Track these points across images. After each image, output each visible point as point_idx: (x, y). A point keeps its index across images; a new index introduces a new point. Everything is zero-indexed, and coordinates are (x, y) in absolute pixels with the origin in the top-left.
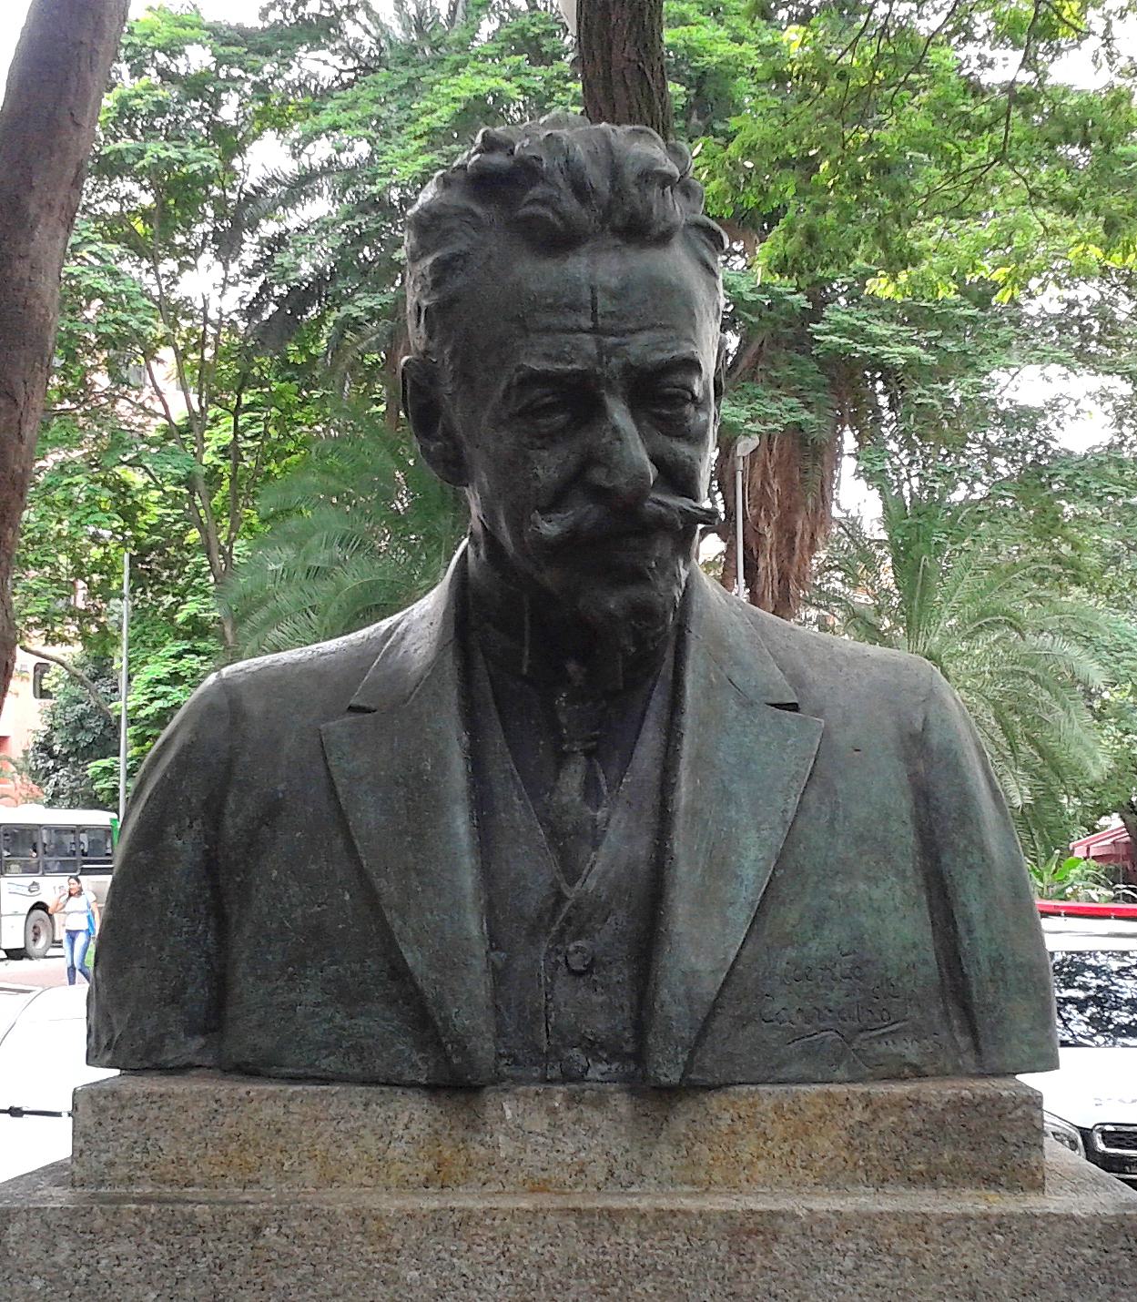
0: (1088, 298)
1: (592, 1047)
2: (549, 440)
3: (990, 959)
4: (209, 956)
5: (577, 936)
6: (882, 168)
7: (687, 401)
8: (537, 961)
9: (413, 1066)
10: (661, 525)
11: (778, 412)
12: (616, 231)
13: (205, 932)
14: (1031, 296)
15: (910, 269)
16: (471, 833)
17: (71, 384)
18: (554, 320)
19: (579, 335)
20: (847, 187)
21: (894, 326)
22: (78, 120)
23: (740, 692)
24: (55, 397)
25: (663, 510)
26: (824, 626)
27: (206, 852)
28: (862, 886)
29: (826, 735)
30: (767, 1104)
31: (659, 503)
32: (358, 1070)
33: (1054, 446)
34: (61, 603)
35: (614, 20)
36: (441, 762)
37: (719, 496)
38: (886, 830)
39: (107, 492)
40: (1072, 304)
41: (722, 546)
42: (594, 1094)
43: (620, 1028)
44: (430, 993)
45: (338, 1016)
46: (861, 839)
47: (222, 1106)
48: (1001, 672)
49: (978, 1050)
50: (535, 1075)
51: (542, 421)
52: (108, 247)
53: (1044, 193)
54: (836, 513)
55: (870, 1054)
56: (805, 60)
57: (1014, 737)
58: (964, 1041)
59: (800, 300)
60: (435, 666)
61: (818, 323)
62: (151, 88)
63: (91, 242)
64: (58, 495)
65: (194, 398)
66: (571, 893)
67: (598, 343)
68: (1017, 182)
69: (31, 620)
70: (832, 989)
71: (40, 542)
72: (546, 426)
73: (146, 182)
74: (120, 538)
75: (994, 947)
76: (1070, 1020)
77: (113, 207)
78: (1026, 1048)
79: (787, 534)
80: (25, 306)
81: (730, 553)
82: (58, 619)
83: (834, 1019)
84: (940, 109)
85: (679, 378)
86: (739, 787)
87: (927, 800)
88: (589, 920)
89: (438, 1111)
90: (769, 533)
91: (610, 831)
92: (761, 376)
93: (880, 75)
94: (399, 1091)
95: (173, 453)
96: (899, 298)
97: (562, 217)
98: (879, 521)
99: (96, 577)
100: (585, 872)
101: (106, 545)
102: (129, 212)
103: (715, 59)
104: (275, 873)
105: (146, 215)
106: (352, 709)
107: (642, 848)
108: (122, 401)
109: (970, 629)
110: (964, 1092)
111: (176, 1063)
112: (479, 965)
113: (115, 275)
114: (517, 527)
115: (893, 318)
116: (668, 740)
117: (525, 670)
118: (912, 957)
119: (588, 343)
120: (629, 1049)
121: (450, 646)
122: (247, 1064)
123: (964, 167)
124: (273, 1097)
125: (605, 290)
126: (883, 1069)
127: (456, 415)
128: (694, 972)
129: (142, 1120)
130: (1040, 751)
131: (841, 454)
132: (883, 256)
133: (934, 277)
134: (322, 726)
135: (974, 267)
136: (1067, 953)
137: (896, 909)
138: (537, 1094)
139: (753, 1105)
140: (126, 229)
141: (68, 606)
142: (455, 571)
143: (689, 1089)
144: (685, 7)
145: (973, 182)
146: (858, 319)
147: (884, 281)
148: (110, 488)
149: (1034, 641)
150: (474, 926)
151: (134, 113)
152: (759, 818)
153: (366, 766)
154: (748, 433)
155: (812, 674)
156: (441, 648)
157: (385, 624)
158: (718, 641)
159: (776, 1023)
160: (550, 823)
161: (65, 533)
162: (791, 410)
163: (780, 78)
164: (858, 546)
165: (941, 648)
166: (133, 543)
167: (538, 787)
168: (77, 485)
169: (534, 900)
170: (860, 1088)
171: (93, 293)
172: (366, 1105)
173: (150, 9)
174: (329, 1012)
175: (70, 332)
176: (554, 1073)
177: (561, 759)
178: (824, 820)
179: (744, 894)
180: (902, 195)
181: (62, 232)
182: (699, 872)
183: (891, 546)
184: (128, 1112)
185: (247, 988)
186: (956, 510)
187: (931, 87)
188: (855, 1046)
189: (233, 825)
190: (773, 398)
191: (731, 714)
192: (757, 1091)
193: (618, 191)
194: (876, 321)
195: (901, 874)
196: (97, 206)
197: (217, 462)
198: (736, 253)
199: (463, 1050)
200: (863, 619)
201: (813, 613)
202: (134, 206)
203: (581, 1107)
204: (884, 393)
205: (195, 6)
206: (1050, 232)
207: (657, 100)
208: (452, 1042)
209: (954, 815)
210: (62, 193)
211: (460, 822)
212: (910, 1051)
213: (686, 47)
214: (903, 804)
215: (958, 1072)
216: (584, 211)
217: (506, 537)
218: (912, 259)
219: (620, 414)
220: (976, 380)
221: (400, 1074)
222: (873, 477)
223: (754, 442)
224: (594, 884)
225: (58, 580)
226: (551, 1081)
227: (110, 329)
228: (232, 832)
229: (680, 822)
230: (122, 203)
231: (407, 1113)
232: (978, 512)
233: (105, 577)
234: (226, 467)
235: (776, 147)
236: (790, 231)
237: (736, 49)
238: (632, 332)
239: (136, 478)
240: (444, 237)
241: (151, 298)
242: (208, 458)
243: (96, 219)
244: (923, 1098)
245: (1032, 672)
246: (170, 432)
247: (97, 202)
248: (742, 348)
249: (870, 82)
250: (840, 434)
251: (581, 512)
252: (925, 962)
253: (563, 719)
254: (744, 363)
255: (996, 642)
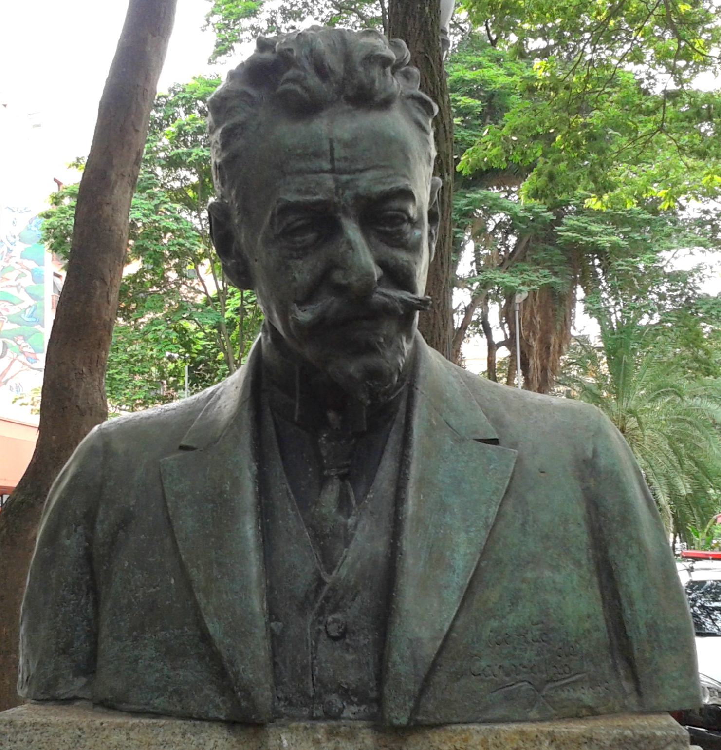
0: (715, 209)
1: (346, 694)
2: (304, 251)
3: (647, 625)
4: (89, 621)
5: (334, 610)
6: (591, 137)
7: (404, 221)
8: (305, 629)
9: (217, 707)
10: (386, 311)
11: (537, 279)
12: (349, 100)
13: (87, 604)
14: (682, 208)
15: (609, 193)
16: (256, 536)
17: (157, 278)
18: (303, 165)
19: (322, 175)
20: (572, 149)
21: (604, 226)
22: (137, 128)
23: (454, 431)
24: (149, 285)
25: (387, 300)
26: (568, 396)
27: (86, 548)
28: (547, 573)
29: (519, 461)
30: (476, 739)
31: (385, 295)
32: (179, 708)
33: (698, 291)
34: (153, 393)
35: (409, 28)
36: (236, 484)
37: (506, 325)
38: (565, 530)
39: (175, 334)
40: (706, 212)
41: (508, 353)
42: (348, 729)
43: (366, 678)
44: (225, 655)
45: (166, 668)
46: (547, 537)
47: (84, 733)
48: (672, 419)
49: (640, 694)
50: (304, 713)
51: (298, 239)
52: (174, 205)
53: (686, 148)
54: (573, 332)
55: (557, 699)
56: (545, 79)
57: (681, 456)
58: (628, 686)
59: (550, 215)
60: (236, 417)
61: (559, 226)
62: (194, 119)
63: (166, 203)
64: (150, 336)
65: (220, 283)
66: (328, 579)
67: (336, 181)
68: (670, 142)
69: (138, 402)
70: (525, 650)
71: (141, 361)
72: (300, 242)
73: (194, 170)
74: (183, 357)
75: (650, 616)
76: (716, 620)
77: (177, 184)
78: (676, 692)
79: (546, 345)
80: (110, 230)
81: (513, 357)
82: (150, 401)
83: (526, 673)
84: (623, 103)
85: (396, 204)
86: (454, 502)
87: (597, 507)
88: (342, 598)
89: (234, 739)
90: (535, 344)
91: (357, 533)
92: (528, 259)
93: (589, 86)
94: (207, 724)
95: (209, 311)
96: (604, 209)
97: (307, 89)
98: (599, 337)
99: (172, 379)
100: (339, 564)
101: (176, 362)
102: (185, 186)
103: (498, 86)
104: (126, 564)
105: (194, 187)
106: (182, 448)
107: (380, 546)
108: (184, 286)
109: (653, 395)
110: (628, 733)
111: (66, 696)
112: (260, 633)
113: (177, 220)
114: (284, 314)
115: (603, 222)
116: (400, 467)
117: (296, 418)
118: (587, 625)
119: (329, 181)
120: (373, 695)
121: (247, 403)
122: (106, 700)
123: (639, 135)
124: (120, 726)
125: (340, 141)
126: (565, 710)
127: (242, 237)
128: (418, 640)
129: (30, 742)
130: (697, 464)
131: (575, 300)
132: (594, 186)
133: (624, 196)
134: (161, 460)
135: (647, 190)
136: (715, 581)
137: (574, 589)
138: (306, 728)
139: (465, 740)
140: (184, 196)
141: (157, 394)
142: (254, 351)
143: (416, 727)
144: (480, 59)
145: (645, 143)
146: (583, 223)
147: (595, 200)
148: (177, 332)
149: (692, 402)
150: (257, 604)
151: (186, 134)
152: (468, 524)
153: (187, 488)
154: (521, 291)
155: (509, 418)
156: (242, 403)
157: (209, 390)
158: (439, 396)
159: (483, 677)
160: (314, 528)
161: (154, 356)
162: (545, 276)
163: (531, 90)
164: (586, 351)
165: (636, 407)
166: (190, 360)
167: (304, 502)
168: (159, 330)
169: (302, 582)
170: (547, 727)
171: (167, 230)
172: (184, 735)
173: (194, 78)
174: (160, 665)
175: (155, 251)
176: (318, 712)
177: (323, 481)
178: (517, 525)
179: (456, 579)
180: (603, 152)
181: (129, 190)
182: (422, 563)
183: (607, 351)
184: (19, 736)
185: (109, 648)
186: (642, 329)
187: (619, 91)
188: (544, 693)
189: (101, 530)
190: (536, 271)
191: (447, 448)
192: (468, 729)
193: (350, 71)
194: (593, 224)
195: (578, 564)
196: (168, 184)
197: (234, 316)
198: (514, 192)
199: (248, 696)
200: (591, 391)
201: (562, 388)
202: (189, 183)
203: (338, 739)
204: (599, 266)
205: (217, 75)
206: (692, 169)
207: (437, 77)
208: (240, 690)
209: (618, 519)
210: (129, 169)
211: (249, 528)
212: (587, 696)
213: (482, 80)
214: (578, 511)
215: (625, 710)
216: (324, 86)
217: (279, 326)
218: (609, 187)
219: (353, 231)
220: (652, 256)
221: (207, 712)
222: (598, 313)
223: (525, 295)
224: (345, 573)
225: (152, 381)
226: (317, 719)
227: (176, 248)
228: (101, 535)
229: (408, 527)
230: (182, 182)
231: (212, 741)
232: (656, 331)
233: (175, 379)
234: (237, 318)
235: (530, 128)
236: (539, 175)
237: (509, 80)
238: (361, 171)
239: (191, 326)
240: (230, 112)
241: (197, 231)
242: (228, 314)
243: (168, 190)
244: (595, 736)
245: (689, 419)
246: (209, 301)
247: (168, 182)
248: (517, 245)
249: (584, 90)
250: (575, 289)
251: (328, 303)
252: (597, 629)
253: (324, 453)
254: (518, 252)
255: (669, 402)
